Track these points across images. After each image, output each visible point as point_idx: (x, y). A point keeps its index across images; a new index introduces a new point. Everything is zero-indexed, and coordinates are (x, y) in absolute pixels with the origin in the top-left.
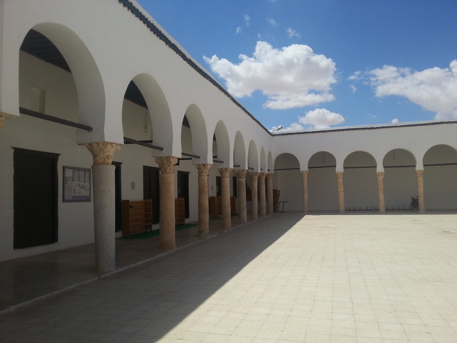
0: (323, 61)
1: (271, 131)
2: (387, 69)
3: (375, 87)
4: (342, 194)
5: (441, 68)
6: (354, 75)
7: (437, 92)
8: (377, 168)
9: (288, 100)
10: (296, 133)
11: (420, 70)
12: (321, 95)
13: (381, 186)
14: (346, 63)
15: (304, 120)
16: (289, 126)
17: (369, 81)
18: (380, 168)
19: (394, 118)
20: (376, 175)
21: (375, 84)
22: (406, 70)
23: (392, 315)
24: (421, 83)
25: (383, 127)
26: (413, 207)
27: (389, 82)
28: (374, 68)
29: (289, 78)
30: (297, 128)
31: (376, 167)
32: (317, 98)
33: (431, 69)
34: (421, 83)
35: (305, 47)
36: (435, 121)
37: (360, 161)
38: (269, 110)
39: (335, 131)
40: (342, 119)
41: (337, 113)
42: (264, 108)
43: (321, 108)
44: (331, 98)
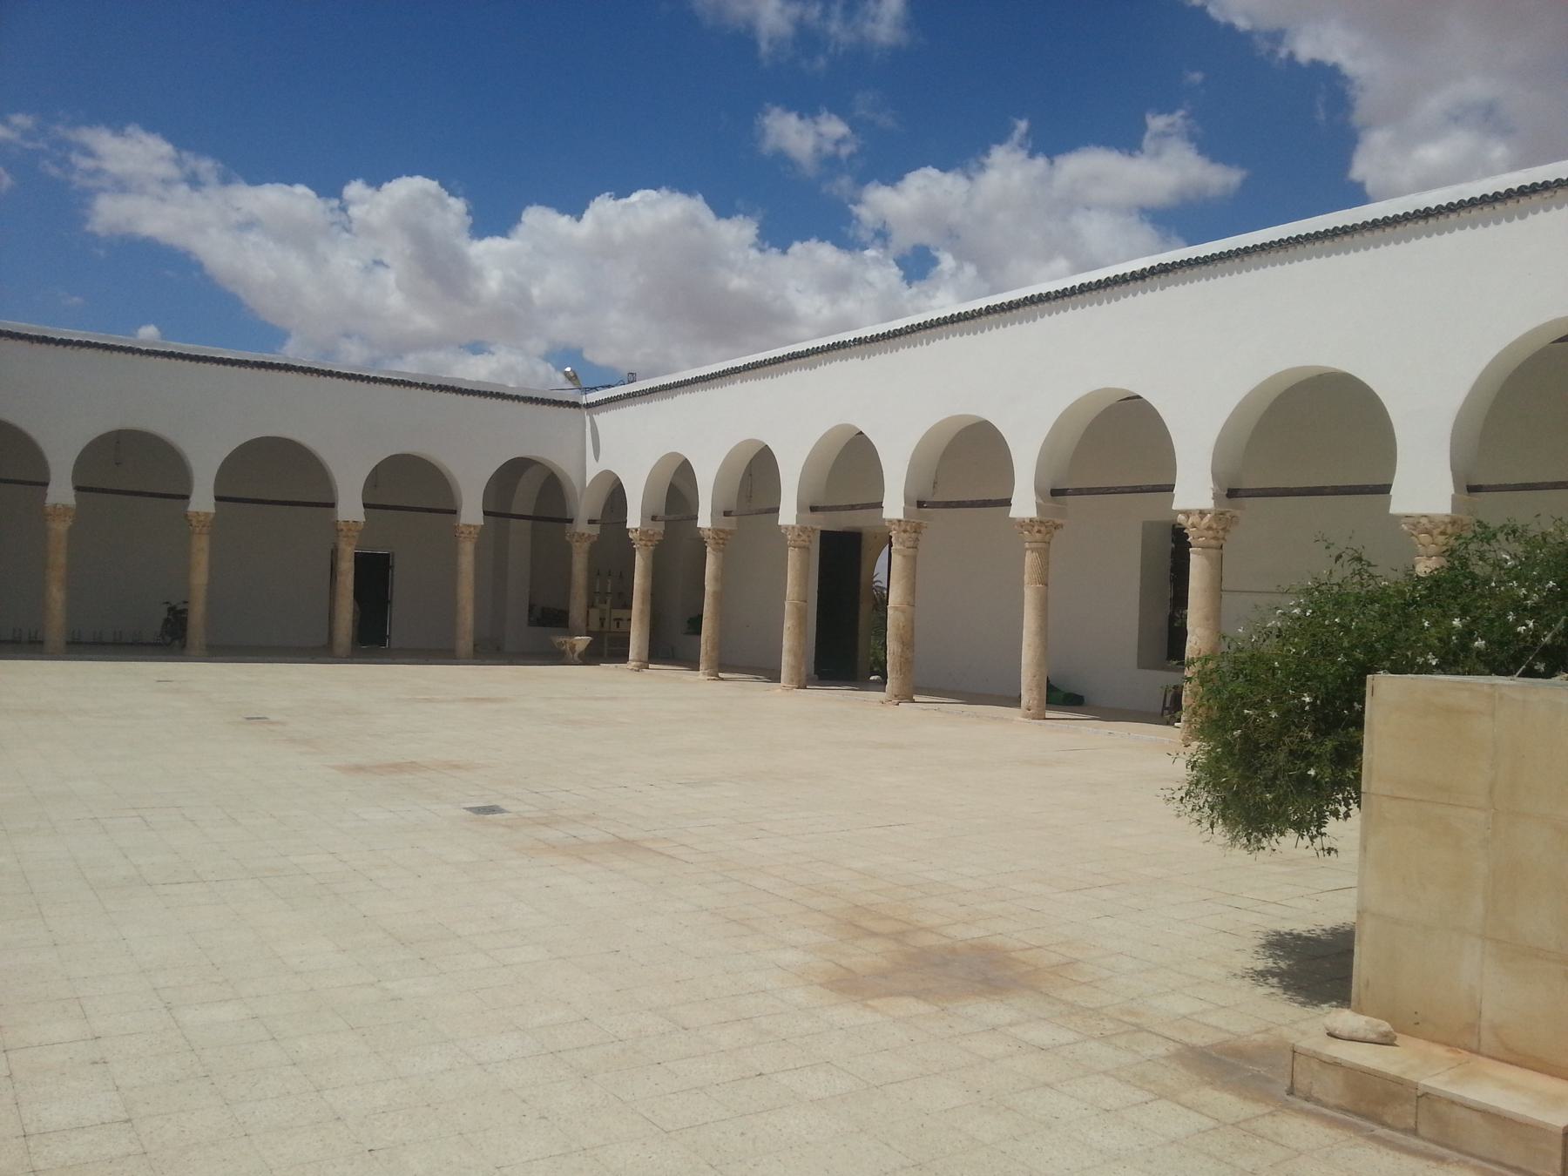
5: (319, 195)
7: (297, 266)
8: (51, 489)
18: (61, 492)
19: (146, 322)
20: (454, 534)
21: (90, 183)
22: (206, 166)
24: (249, 224)
25: (88, 345)
26: (169, 637)
31: (46, 484)
33: (286, 187)
34: (249, 224)
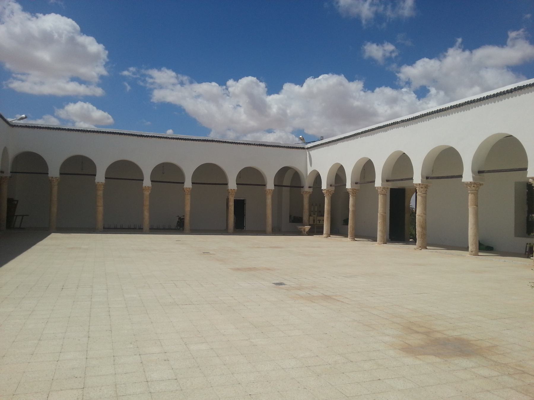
0: (92, 45)
1: (9, 120)
2: (166, 72)
3: (152, 90)
4: (100, 209)
5: (220, 85)
6: (128, 70)
7: (213, 108)
8: (144, 182)
9: (42, 83)
10: (46, 128)
11: (200, 82)
12: (87, 87)
13: (147, 203)
14: (120, 55)
15: (62, 113)
16: (41, 118)
17: (144, 81)
18: (147, 182)
19: (170, 129)
21: (152, 86)
22: (185, 78)
23: (132, 346)
24: (199, 96)
25: (154, 137)
26: (179, 227)
27: (166, 88)
28: (152, 67)
29: (44, 55)
30: (53, 122)
31: (143, 180)
32: (82, 89)
34: (199, 96)
35: (70, 21)
36: (206, 138)
37: (124, 172)
38: (13, 92)
39: (101, 132)
40: (111, 120)
41: (105, 112)
42: (5, 87)
43: (85, 102)
44: (99, 92)
